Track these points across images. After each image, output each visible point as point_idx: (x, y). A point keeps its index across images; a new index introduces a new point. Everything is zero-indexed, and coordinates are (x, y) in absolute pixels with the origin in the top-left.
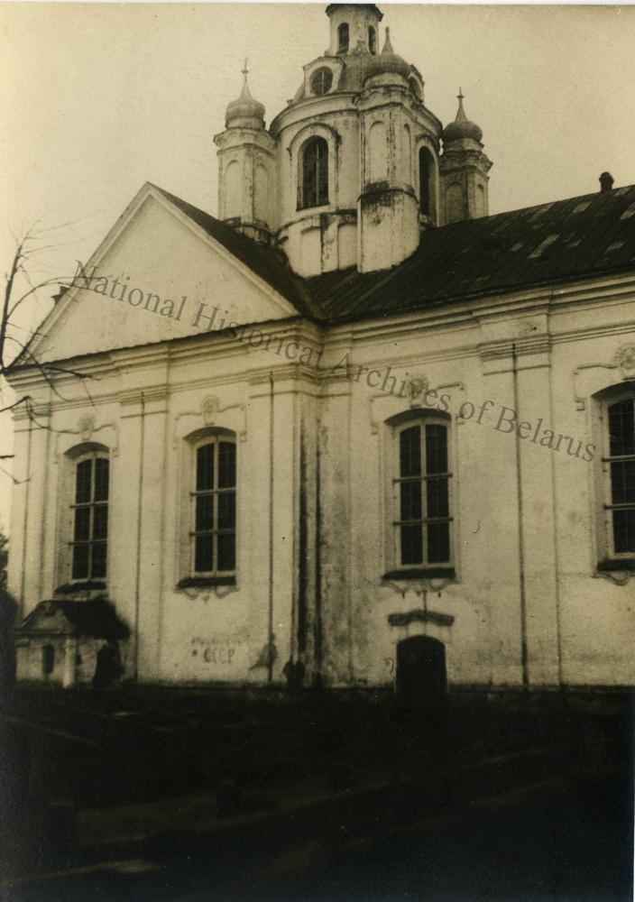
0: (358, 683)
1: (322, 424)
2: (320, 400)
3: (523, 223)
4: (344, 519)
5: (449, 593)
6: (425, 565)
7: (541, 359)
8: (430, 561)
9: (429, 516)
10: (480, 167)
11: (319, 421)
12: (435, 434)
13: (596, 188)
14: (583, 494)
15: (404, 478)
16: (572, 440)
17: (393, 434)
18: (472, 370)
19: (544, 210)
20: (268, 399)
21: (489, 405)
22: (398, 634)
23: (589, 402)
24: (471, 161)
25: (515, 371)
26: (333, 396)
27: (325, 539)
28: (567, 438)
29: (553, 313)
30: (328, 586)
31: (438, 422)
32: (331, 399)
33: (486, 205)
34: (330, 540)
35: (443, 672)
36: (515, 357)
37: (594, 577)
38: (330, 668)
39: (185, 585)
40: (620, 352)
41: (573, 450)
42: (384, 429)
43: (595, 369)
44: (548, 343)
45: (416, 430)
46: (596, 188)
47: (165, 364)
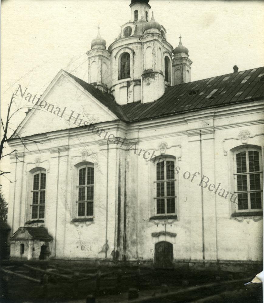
0: (139, 259)
1: (127, 160)
2: (126, 152)
3: (204, 85)
4: (135, 197)
5: (175, 225)
7: (211, 136)
8: (168, 212)
10: (188, 64)
11: (126, 159)
12: (253, 155)
13: (232, 71)
15: (158, 181)
18: (184, 140)
19: (212, 80)
21: (197, 173)
22: (156, 240)
24: (184, 61)
25: (201, 141)
27: (128, 204)
28: (144, 150)
30: (129, 222)
33: (190, 79)
34: (129, 204)
35: (172, 255)
36: (200, 135)
37: (230, 219)
38: (129, 253)
39: (235, 215)
40: (241, 133)
44: (214, 130)
46: (232, 71)
47: (68, 138)
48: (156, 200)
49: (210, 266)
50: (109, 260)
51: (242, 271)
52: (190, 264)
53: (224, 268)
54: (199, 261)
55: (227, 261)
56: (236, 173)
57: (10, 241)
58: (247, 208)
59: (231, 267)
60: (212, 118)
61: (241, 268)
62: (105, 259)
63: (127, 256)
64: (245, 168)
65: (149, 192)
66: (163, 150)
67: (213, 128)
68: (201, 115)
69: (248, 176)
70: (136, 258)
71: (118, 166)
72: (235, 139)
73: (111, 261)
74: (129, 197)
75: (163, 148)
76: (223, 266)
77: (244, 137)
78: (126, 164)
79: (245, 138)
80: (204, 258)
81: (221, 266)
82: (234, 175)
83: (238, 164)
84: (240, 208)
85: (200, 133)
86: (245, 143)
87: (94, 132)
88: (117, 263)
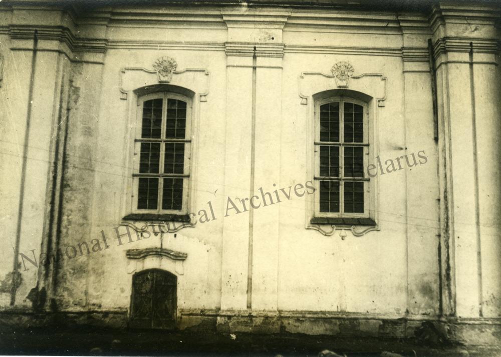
1: (74, 84)
2: (74, 64)
4: (88, 167)
5: (184, 235)
6: (160, 211)
8: (164, 208)
9: (165, 172)
11: (71, 81)
14: (302, 166)
16: (406, 156)
17: (138, 101)
18: (216, 61)
20: (31, 53)
22: (137, 266)
23: (311, 100)
25: (255, 68)
26: (87, 62)
27: (70, 183)
28: (247, 199)
29: (111, 25)
31: (179, 98)
32: (85, 65)
34: (74, 183)
35: (174, 300)
36: (255, 57)
38: (66, 294)
39: (317, 222)
41: (411, 162)
42: (132, 97)
43: (138, 72)
44: (281, 51)
45: (159, 102)
48: (136, 180)
49: (264, 323)
50: (22, 312)
51: (328, 333)
52: (219, 318)
53: (292, 327)
54: (240, 311)
55: (297, 312)
56: (318, 141)
57: (8, 282)
58: (338, 211)
59: (307, 324)
60: (282, 27)
61: (327, 326)
62: (11, 307)
63: (61, 301)
64: (337, 134)
65: (125, 159)
66: (164, 74)
67: (283, 47)
68: (260, 16)
69: (342, 150)
70: (84, 307)
71: (59, 95)
72: (325, 76)
73: (28, 314)
74: (74, 167)
75: (166, 70)
76: (290, 322)
77: (343, 74)
78: (71, 93)
79: (344, 78)
80: (249, 307)
81: (286, 322)
82: (315, 144)
83: (323, 123)
84: (323, 208)
85: (255, 53)
86: (343, 87)
87: (460, 49)
88: (43, 317)
